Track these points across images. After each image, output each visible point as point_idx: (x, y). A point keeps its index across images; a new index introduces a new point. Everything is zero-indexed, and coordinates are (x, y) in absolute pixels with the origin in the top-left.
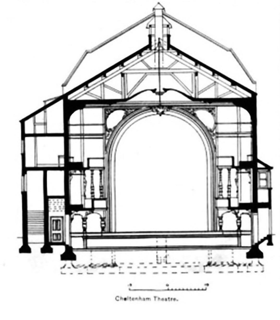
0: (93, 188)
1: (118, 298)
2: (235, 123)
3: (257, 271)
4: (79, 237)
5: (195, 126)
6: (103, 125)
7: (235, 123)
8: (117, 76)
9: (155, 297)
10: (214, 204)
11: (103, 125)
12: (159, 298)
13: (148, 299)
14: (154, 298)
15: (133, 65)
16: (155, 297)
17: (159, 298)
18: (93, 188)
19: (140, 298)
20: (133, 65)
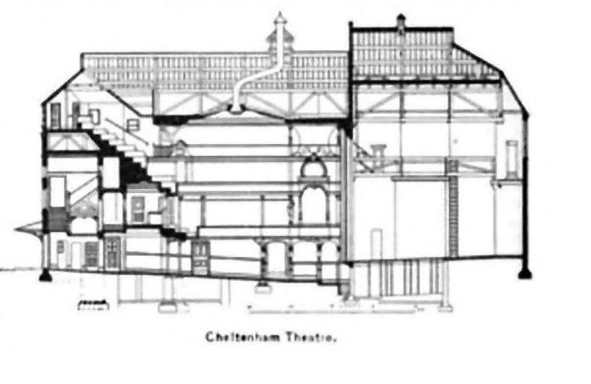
0: (60, 245)
1: (210, 337)
2: (156, 255)
3: (383, 143)
4: (392, 272)
5: (413, 276)
6: (369, 266)
7: (156, 255)
8: (76, 187)
9: (289, 333)
10: (425, 259)
11: (369, 266)
12: (296, 336)
13: (275, 338)
14: (286, 337)
15: (86, 184)
16: (289, 333)
17: (296, 336)
18: (60, 245)
19: (257, 336)
20: (86, 184)
